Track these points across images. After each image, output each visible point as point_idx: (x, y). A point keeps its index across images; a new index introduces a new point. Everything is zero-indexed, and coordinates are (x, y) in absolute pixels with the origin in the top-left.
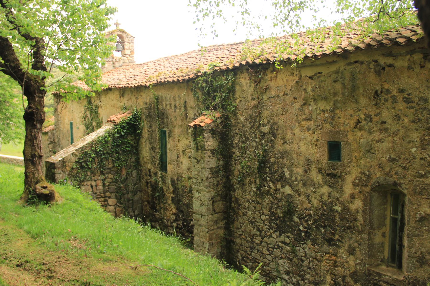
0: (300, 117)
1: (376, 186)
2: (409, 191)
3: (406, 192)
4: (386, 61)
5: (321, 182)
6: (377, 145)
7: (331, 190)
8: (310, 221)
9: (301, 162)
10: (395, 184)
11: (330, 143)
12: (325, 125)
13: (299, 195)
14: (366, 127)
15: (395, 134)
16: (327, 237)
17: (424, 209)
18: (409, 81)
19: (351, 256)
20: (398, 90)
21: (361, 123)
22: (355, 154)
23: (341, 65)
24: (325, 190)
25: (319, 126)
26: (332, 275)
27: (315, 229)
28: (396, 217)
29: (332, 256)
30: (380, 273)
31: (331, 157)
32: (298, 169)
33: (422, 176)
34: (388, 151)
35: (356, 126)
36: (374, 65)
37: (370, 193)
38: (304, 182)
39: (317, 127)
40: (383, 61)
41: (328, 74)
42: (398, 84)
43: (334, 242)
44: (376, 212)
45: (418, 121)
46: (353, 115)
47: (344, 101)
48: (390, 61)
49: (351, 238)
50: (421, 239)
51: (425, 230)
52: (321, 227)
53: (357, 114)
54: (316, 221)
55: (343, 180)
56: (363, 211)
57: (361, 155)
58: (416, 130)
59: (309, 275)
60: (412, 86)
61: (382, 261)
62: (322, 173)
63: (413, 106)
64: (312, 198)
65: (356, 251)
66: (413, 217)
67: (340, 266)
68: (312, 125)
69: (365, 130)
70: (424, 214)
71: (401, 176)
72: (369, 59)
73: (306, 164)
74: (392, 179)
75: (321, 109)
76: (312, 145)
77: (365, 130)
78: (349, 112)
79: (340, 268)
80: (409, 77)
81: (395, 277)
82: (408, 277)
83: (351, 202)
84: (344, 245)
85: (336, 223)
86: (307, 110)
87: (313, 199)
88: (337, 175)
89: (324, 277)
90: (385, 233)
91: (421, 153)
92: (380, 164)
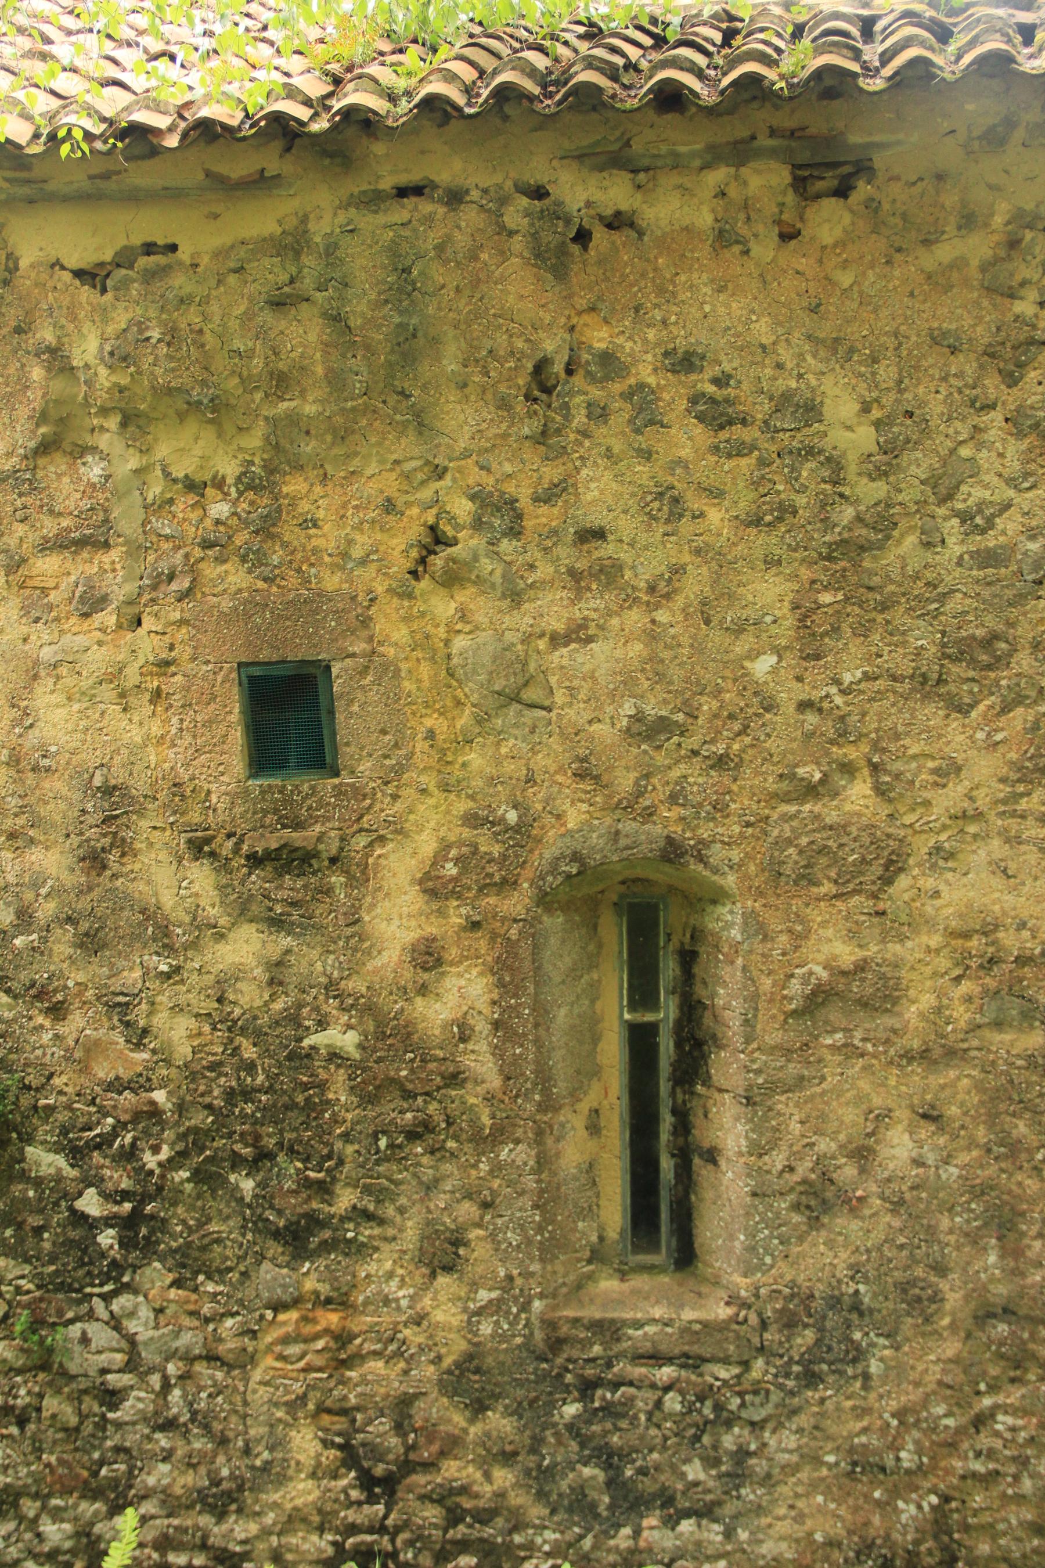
0: (20, 529)
1: (569, 876)
2: (746, 877)
3: (730, 881)
4: (598, 196)
5: (213, 912)
6: (561, 656)
7: (287, 941)
8: (156, 1150)
9: (54, 811)
10: (672, 851)
11: (256, 671)
12: (210, 571)
13: (57, 1012)
14: (486, 565)
15: (660, 592)
16: (280, 1213)
17: (825, 949)
18: (722, 310)
19: (443, 1280)
20: (666, 354)
21: (454, 542)
22: (429, 722)
23: (319, 205)
24: (245, 948)
25: (171, 577)
26: (326, 1419)
27: (189, 1187)
28: (649, 1017)
29: (319, 1313)
30: (613, 1321)
31: (266, 754)
32: (35, 856)
33: (811, 791)
34: (627, 683)
35: (423, 561)
36: (527, 214)
37: (529, 922)
38: (84, 926)
39: (154, 587)
40: (580, 192)
41: (219, 254)
42: (664, 322)
43: (327, 1234)
44: (563, 1012)
45: (780, 519)
46: (400, 500)
47: (339, 420)
48: (615, 193)
49: (430, 1187)
50: (813, 1097)
51: (833, 1048)
52: (233, 1168)
53: (426, 494)
54: (194, 1140)
55: (360, 876)
56: (496, 1025)
57: (460, 723)
58: (772, 562)
59: (164, 1468)
60: (738, 335)
61: (596, 1256)
62: (213, 854)
63: (748, 439)
64: (150, 1014)
65: (466, 1244)
66: (771, 1001)
67: (376, 1354)
68: (113, 571)
69: (479, 581)
70: (824, 975)
71: (700, 805)
72: (498, 178)
73: (97, 818)
74: (657, 830)
75: (178, 472)
76: (122, 695)
77: (479, 581)
78: (371, 489)
79: (377, 1366)
80: (720, 290)
81: (688, 1314)
82: (757, 1296)
83: (423, 990)
84: (391, 1232)
85: (335, 1121)
86: (69, 486)
87: (160, 1020)
88: (315, 854)
89: (271, 1449)
90: (597, 1111)
91: (799, 679)
92: (584, 760)
